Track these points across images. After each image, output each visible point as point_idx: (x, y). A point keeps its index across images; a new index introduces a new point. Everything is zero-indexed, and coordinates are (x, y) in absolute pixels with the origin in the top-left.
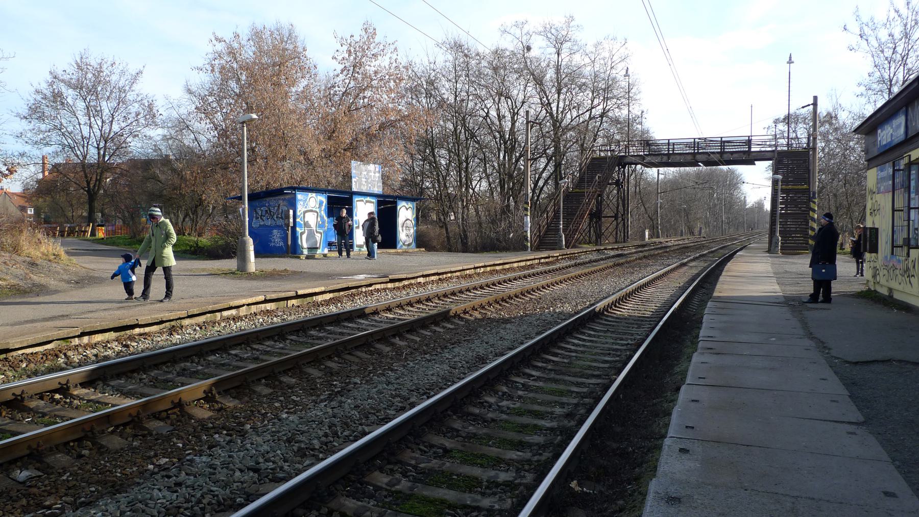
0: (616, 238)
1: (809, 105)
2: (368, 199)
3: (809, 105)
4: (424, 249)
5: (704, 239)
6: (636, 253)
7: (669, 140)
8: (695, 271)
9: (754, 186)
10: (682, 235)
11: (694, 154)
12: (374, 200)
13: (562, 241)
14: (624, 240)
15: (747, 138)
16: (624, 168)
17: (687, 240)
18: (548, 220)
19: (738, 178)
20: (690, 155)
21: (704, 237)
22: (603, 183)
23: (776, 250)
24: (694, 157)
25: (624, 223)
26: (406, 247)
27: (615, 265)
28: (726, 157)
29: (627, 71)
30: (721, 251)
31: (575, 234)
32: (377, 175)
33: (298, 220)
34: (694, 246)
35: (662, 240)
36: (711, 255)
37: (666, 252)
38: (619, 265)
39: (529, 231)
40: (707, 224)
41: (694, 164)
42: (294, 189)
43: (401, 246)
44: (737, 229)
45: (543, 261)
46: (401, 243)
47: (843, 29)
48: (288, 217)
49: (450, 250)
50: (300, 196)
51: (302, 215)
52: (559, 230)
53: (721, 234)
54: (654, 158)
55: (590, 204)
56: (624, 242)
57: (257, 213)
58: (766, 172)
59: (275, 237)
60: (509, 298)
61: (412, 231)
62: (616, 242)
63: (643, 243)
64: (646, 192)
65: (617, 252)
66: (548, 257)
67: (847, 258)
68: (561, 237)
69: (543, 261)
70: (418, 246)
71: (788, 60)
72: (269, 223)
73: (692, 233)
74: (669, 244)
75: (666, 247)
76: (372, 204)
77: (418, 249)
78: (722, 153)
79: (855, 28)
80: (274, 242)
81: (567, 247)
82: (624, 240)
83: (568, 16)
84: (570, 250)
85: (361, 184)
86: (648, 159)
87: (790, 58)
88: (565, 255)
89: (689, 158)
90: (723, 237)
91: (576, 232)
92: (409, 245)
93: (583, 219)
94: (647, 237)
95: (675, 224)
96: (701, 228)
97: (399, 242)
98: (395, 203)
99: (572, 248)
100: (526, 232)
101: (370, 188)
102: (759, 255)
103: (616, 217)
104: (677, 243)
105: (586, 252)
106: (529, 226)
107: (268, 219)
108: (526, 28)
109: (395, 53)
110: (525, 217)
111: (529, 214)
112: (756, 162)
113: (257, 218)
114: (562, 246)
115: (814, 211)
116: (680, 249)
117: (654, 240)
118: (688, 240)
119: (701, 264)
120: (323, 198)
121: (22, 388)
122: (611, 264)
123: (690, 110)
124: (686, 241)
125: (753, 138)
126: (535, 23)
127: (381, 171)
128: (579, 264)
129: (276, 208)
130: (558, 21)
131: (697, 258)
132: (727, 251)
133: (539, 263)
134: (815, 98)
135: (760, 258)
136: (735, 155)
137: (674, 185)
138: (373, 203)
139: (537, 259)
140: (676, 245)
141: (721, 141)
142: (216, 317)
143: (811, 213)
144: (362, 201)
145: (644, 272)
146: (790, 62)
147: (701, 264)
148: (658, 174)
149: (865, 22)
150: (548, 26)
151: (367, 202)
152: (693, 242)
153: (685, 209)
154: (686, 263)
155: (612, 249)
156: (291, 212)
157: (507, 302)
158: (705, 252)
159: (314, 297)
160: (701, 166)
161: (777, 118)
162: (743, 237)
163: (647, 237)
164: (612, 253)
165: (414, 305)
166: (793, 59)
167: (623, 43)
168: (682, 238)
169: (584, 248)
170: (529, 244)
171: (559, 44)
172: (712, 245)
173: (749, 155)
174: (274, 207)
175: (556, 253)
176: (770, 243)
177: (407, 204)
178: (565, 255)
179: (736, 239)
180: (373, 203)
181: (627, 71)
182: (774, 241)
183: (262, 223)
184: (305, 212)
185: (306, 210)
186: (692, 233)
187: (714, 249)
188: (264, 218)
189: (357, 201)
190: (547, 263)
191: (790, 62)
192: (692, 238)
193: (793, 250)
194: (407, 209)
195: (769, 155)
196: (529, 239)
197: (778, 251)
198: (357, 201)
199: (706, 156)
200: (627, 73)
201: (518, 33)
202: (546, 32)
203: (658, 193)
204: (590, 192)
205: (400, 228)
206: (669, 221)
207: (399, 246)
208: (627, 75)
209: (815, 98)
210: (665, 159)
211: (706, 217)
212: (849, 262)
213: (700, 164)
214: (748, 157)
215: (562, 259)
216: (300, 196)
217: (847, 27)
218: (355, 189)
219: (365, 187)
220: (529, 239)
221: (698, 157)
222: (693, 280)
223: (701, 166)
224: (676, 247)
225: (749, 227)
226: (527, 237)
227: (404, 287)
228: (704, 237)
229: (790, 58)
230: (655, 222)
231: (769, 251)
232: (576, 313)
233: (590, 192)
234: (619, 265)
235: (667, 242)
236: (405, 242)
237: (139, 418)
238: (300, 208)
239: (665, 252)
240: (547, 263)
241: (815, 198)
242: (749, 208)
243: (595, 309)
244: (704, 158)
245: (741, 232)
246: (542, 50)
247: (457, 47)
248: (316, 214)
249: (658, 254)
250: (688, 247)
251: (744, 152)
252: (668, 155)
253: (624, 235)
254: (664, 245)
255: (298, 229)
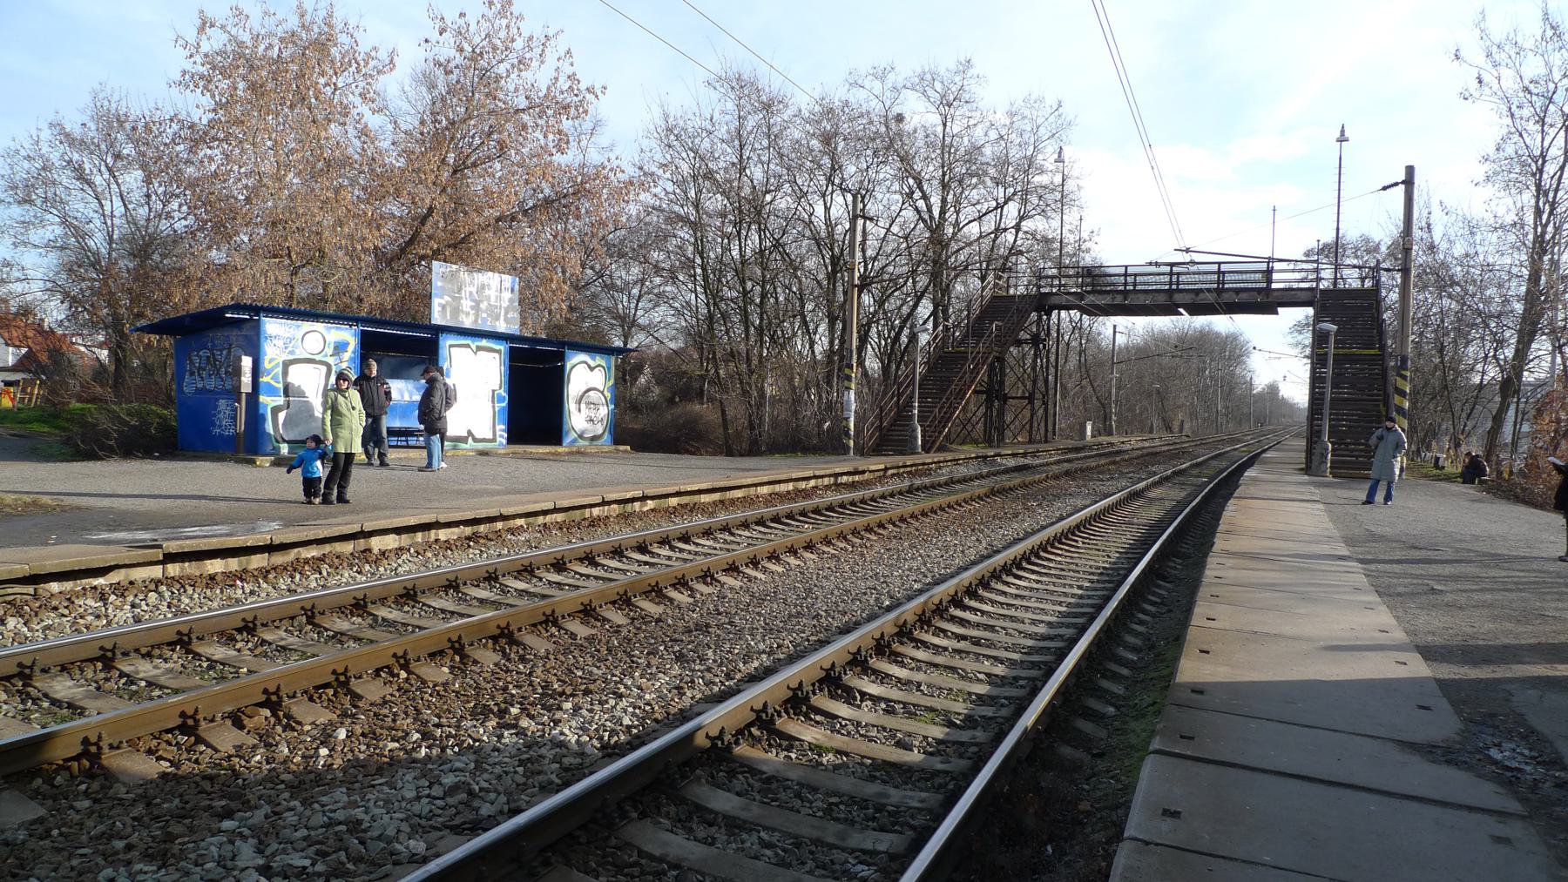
0: (1030, 436)
1: (1396, 184)
2: (484, 343)
3: (1396, 184)
4: (629, 448)
5: (1187, 439)
6: (1058, 462)
7: (1126, 267)
8: (1155, 513)
9: (1272, 355)
10: (1151, 432)
11: (1170, 292)
12: (502, 347)
13: (916, 438)
14: (1046, 436)
15: (1264, 267)
16: (1049, 314)
17: (1158, 441)
18: (899, 400)
19: (1242, 346)
20: (1162, 294)
21: (1187, 436)
22: (1010, 338)
23: (1323, 468)
24: (1171, 297)
25: (1046, 410)
26: (587, 443)
27: (993, 492)
28: (1226, 297)
29: (1060, 153)
30: (1214, 463)
31: (944, 427)
32: (507, 295)
33: (264, 379)
34: (1168, 451)
35: (1114, 439)
36: (1195, 471)
37: (1114, 463)
38: (1003, 491)
39: (852, 419)
40: (1193, 415)
41: (1169, 309)
42: (257, 310)
43: (574, 441)
44: (1240, 423)
45: (845, 479)
46: (573, 435)
47: (1454, 57)
48: (237, 372)
49: (730, 453)
50: (273, 327)
51: (280, 370)
52: (911, 417)
53: (1214, 432)
54: (1100, 297)
55: (978, 373)
56: (1046, 441)
57: (192, 363)
58: (1290, 336)
59: (221, 415)
60: (866, 530)
61: (603, 411)
62: (1030, 442)
63: (1080, 444)
64: (1095, 363)
65: (1021, 461)
66: (856, 472)
67: (1471, 491)
68: (914, 430)
69: (845, 479)
70: (617, 441)
71: (1338, 135)
72: (211, 384)
73: (1169, 429)
74: (1127, 447)
75: (1119, 453)
76: (497, 355)
77: (614, 447)
78: (1220, 291)
79: (1475, 54)
80: (220, 426)
81: (927, 448)
82: (1046, 436)
83: (962, 59)
84: (931, 455)
85: (457, 311)
86: (1090, 299)
87: (1343, 131)
88: (898, 467)
89: (1161, 299)
90: (1219, 437)
91: (948, 421)
92: (594, 438)
93: (962, 399)
94: (1089, 433)
95: (1141, 414)
96: (1182, 421)
97: (567, 433)
98: (561, 357)
99: (935, 452)
100: (847, 419)
101: (484, 320)
102: (1289, 478)
103: (1031, 399)
104: (1140, 445)
105: (962, 461)
106: (853, 407)
107: (210, 375)
108: (891, 77)
109: (568, 61)
110: (846, 393)
111: (853, 386)
112: (1279, 309)
113: (192, 374)
114: (916, 446)
115: (1402, 393)
116: (1142, 456)
117: (1104, 439)
118: (1161, 441)
119: (1173, 494)
120: (348, 336)
121: (114, 640)
122: (982, 491)
123: (1154, 164)
124: (1157, 442)
125: (1277, 266)
126: (906, 69)
127: (517, 287)
128: (918, 489)
129: (225, 352)
130: (946, 64)
131: (1167, 479)
132: (1224, 464)
133: (836, 484)
134: (1410, 170)
135: (1293, 488)
136: (1244, 296)
137: (1145, 354)
138: (499, 352)
139: (830, 476)
140: (1137, 449)
141: (1219, 272)
142: (584, 514)
143: (1397, 399)
144: (468, 346)
145: (1059, 507)
146: (1342, 139)
147: (1171, 494)
148: (1115, 332)
149: (1497, 41)
150: (928, 77)
151: (479, 348)
152: (1169, 444)
153: (1159, 392)
154: (1143, 490)
155: (1014, 455)
156: (247, 362)
157: (918, 520)
158: (1184, 466)
159: (433, 532)
160: (1181, 314)
161: (1310, 248)
162: (1249, 438)
163: (1089, 433)
164: (1012, 463)
165: (540, 573)
166: (1347, 134)
167: (1055, 107)
168: (1151, 436)
169: (964, 451)
170: (852, 443)
171: (947, 103)
172: (1200, 450)
173: (1268, 296)
174: (221, 351)
175: (909, 460)
176: (1309, 452)
177: (594, 359)
178: (898, 467)
179: (1239, 441)
180: (499, 352)
181: (1060, 153)
182: (1317, 451)
183: (200, 385)
184: (287, 365)
185: (291, 357)
186: (1169, 429)
187: (1199, 460)
188: (204, 374)
189: (451, 346)
190: (852, 486)
191: (1342, 139)
192: (1167, 436)
193: (1348, 469)
194: (592, 369)
195: (1304, 296)
196: (852, 433)
197: (1325, 471)
198: (451, 346)
199: (1192, 296)
200: (1059, 156)
201: (877, 86)
202: (923, 82)
203: (1113, 363)
204: (978, 353)
205: (571, 405)
206: (1131, 409)
207: (567, 441)
208: (1060, 160)
209: (1410, 170)
210: (1119, 300)
211: (1192, 403)
212: (1481, 501)
213: (1181, 310)
214: (1263, 300)
215: (893, 475)
216: (273, 327)
217: (1462, 54)
218: (437, 318)
219: (471, 318)
220: (852, 433)
221: (1178, 298)
222: (1144, 544)
223: (1181, 314)
224: (1139, 452)
225: (1257, 421)
226: (849, 429)
227: (242, 575)
228: (1187, 436)
229: (1343, 131)
230: (1108, 411)
231: (1307, 470)
232: (611, 752)
233: (978, 353)
234: (1003, 491)
235: (1123, 443)
236: (583, 432)
237: (460, 644)
238: (272, 353)
239: (1115, 461)
240: (852, 486)
241: (1406, 369)
242: (1259, 394)
243: (690, 736)
244: (1188, 298)
245: (1245, 428)
246: (920, 115)
247: (741, 86)
248: (324, 369)
249: (1098, 466)
250: (1157, 453)
251: (1259, 290)
252: (1125, 293)
253: (1046, 431)
254: (1117, 449)
255: (262, 398)
